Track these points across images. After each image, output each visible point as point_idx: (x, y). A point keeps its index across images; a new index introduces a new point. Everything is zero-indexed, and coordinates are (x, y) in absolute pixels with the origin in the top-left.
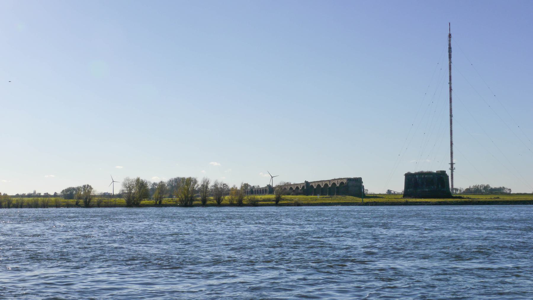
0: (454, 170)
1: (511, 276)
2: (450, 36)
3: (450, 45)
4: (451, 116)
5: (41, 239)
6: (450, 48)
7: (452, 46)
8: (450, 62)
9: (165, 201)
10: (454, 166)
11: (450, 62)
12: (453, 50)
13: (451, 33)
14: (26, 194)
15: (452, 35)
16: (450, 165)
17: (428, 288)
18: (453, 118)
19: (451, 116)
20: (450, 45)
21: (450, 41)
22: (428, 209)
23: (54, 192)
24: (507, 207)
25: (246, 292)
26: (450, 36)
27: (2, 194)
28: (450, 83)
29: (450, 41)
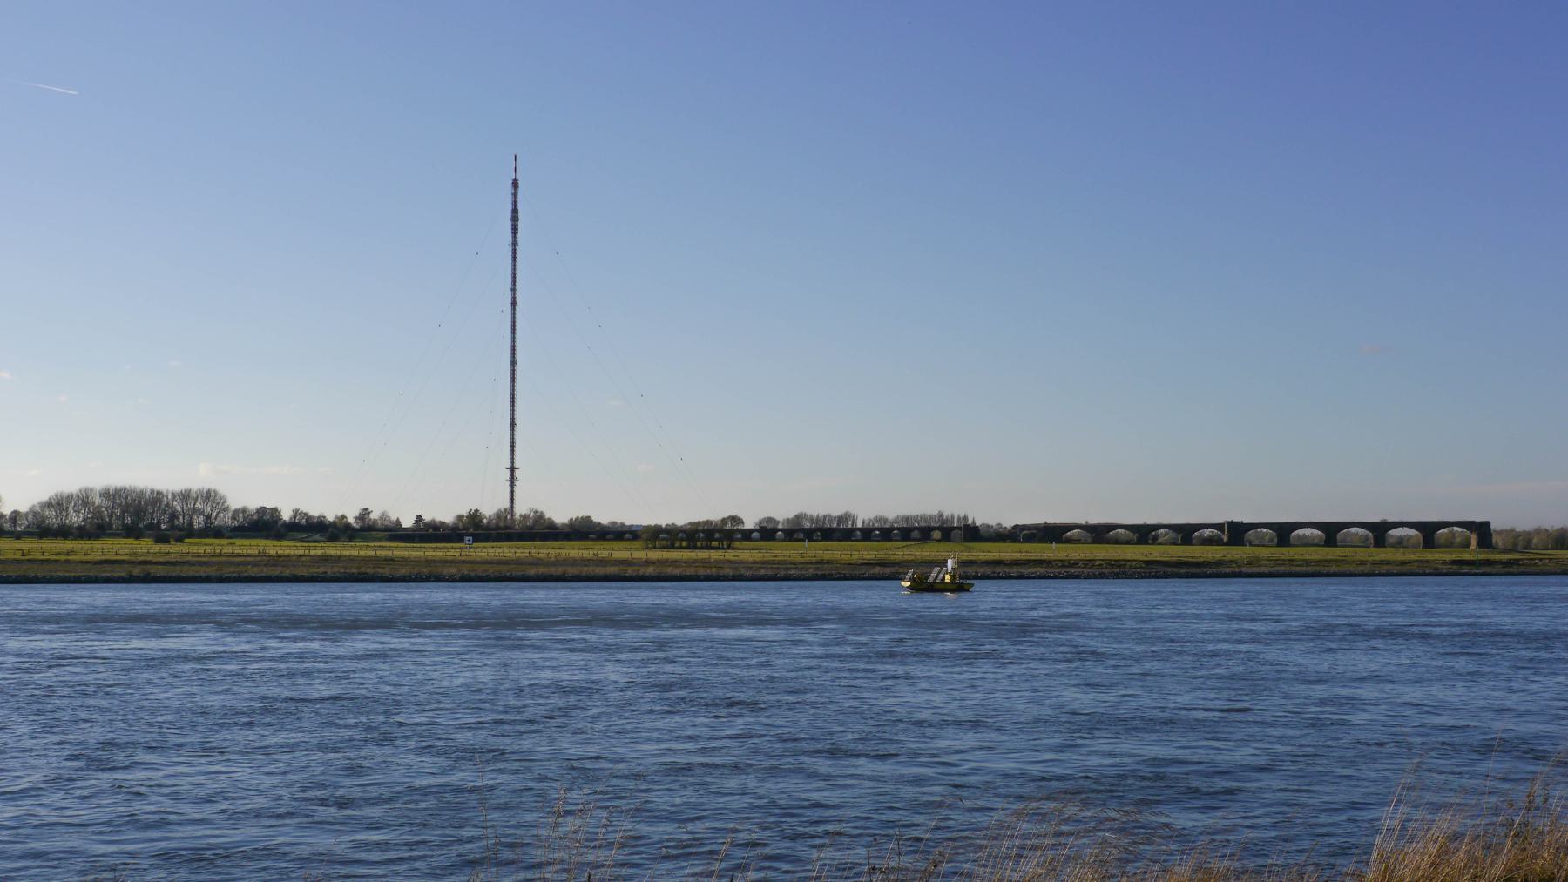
0: (516, 483)
1: (614, 710)
2: (515, 183)
3: (515, 204)
4: (513, 363)
5: (1132, 703)
6: (515, 211)
7: (519, 207)
8: (515, 243)
9: (699, 544)
10: (517, 473)
11: (515, 243)
12: (521, 215)
13: (517, 178)
14: (286, 516)
15: (520, 183)
16: (508, 471)
17: (935, 775)
18: (518, 368)
19: (513, 363)
20: (515, 204)
21: (515, 195)
22: (1531, 591)
23: (1488, 520)
24: (1382, 586)
25: (916, 822)
26: (515, 183)
27: (7, 511)
28: (514, 290)
29: (515, 195)
